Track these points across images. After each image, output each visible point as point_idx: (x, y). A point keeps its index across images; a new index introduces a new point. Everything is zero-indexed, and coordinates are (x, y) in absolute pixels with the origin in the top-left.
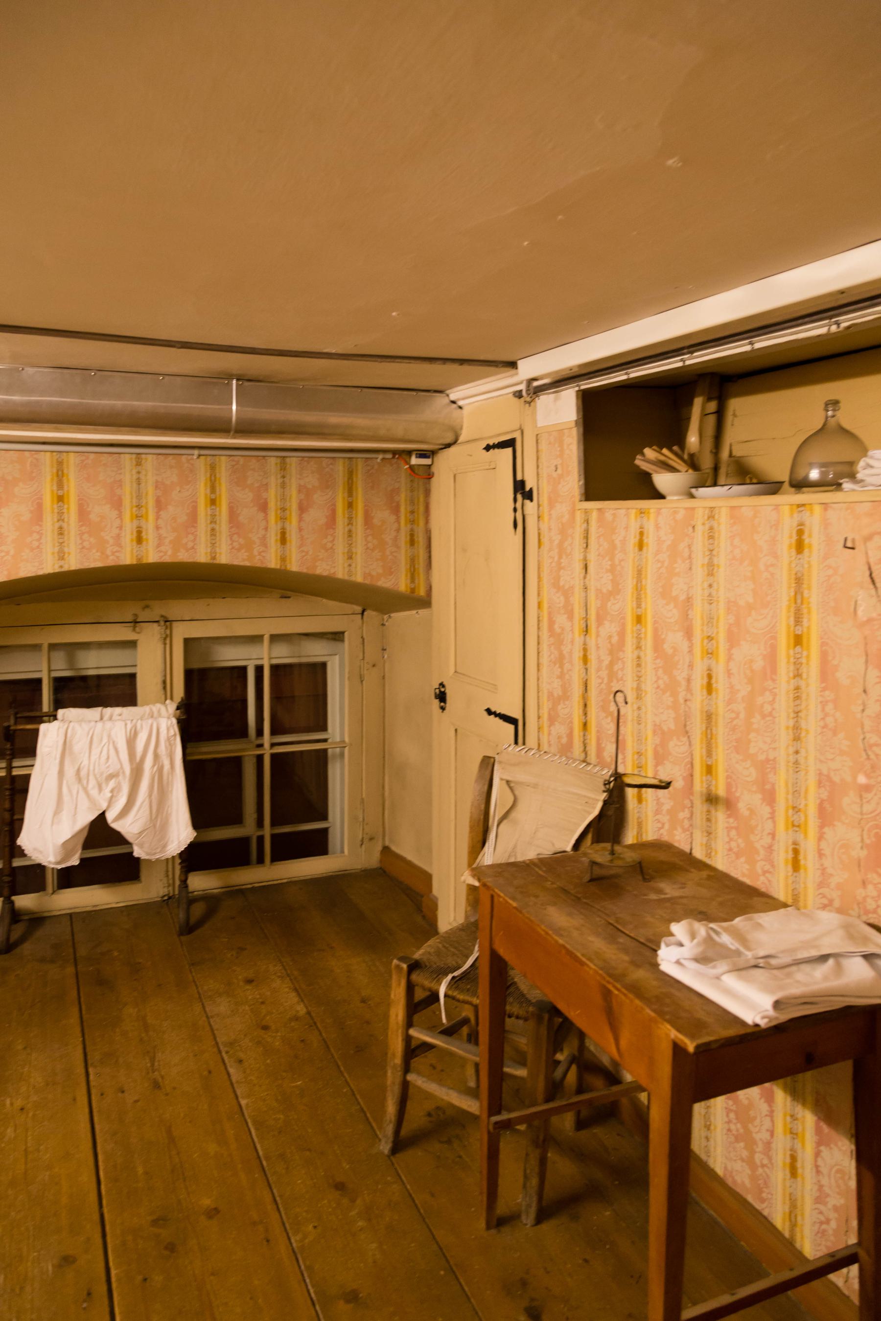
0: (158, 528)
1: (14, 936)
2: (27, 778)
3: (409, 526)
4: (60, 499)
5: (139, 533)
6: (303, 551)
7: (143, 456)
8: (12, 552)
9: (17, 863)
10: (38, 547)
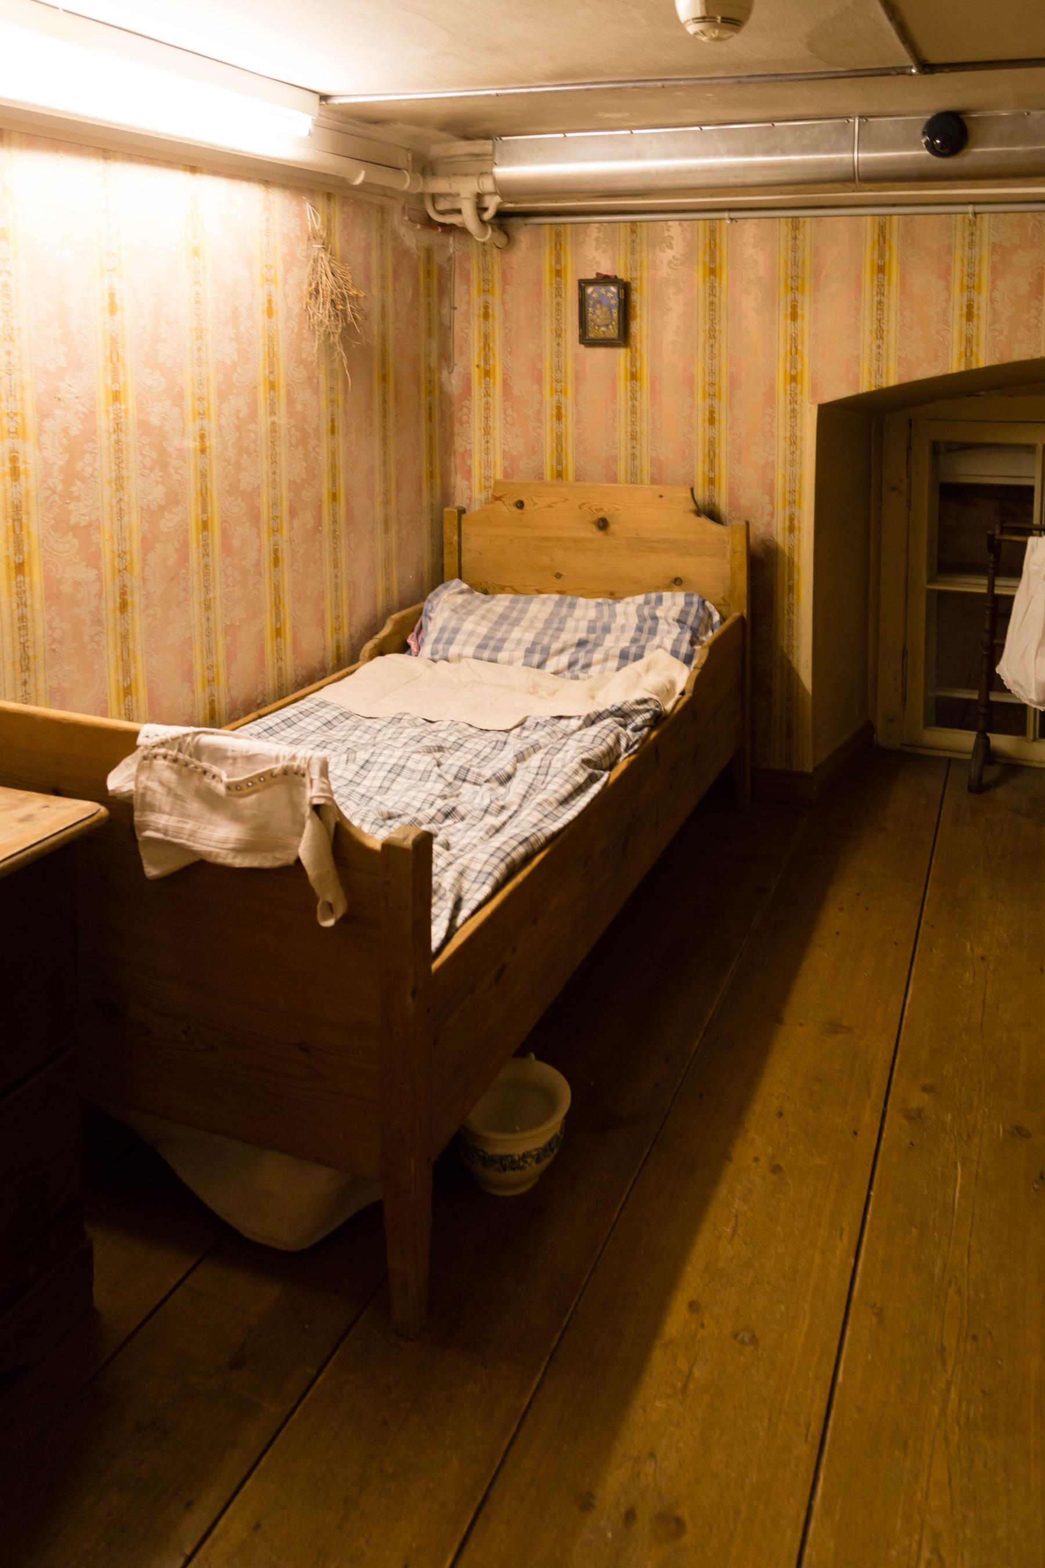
0: (992, 301)
1: (987, 778)
2: (1011, 599)
3: (790, 296)
4: (558, 273)
5: (970, 307)
6: (995, 330)
7: (801, 220)
8: (1005, 332)
9: (995, 697)
10: (1036, 326)
